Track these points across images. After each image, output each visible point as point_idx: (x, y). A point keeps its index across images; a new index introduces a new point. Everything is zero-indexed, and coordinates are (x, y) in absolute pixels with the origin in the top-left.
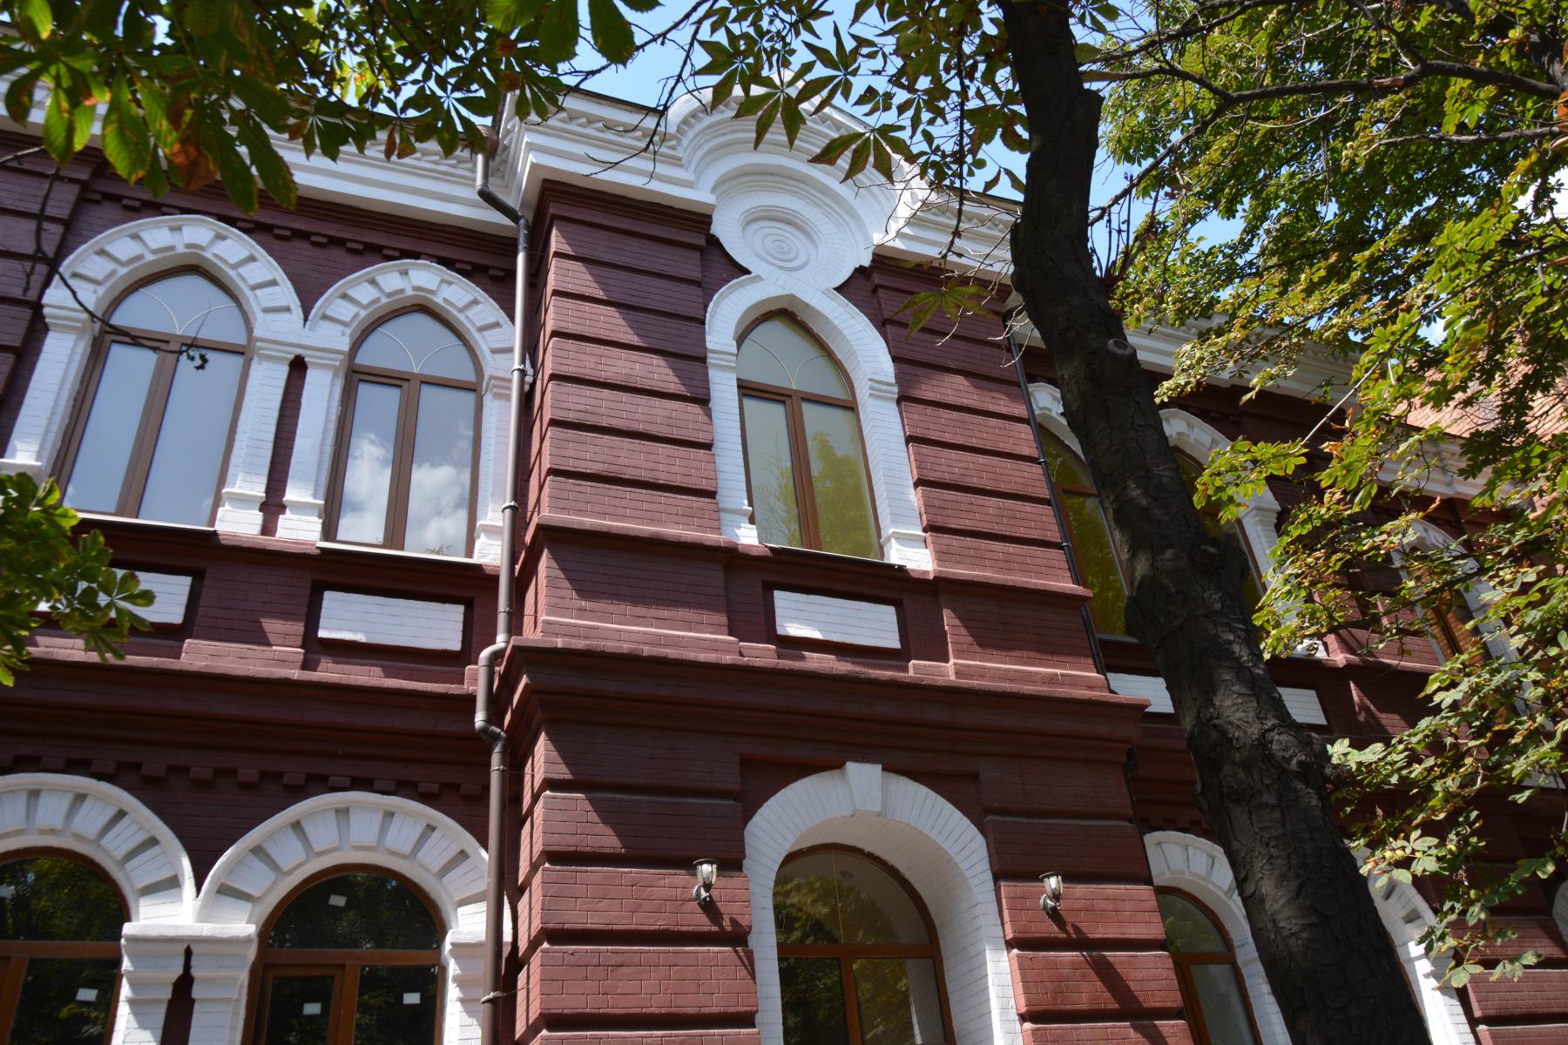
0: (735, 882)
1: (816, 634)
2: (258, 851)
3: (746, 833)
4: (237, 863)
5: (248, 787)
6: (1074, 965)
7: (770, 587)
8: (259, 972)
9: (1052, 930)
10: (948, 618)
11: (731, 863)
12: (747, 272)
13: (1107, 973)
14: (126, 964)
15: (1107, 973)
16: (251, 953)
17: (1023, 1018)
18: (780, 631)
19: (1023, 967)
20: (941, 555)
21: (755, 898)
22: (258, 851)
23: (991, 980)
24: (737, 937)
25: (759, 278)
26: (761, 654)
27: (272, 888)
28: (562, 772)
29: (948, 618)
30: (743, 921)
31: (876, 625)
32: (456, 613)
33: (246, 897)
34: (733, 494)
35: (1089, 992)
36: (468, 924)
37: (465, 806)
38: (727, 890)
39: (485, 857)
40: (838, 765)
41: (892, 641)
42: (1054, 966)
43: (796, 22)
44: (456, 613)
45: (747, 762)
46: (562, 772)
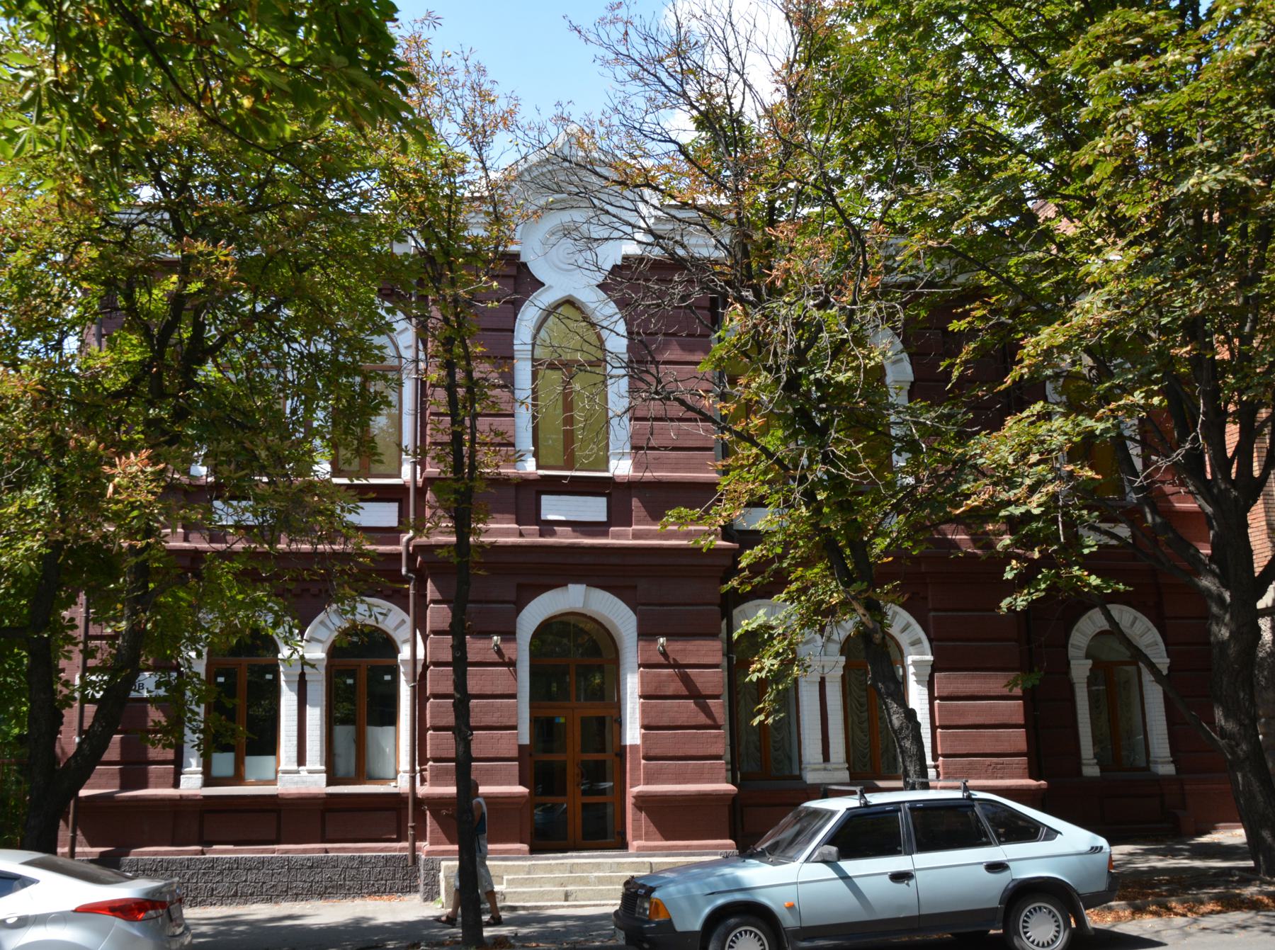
0: (512, 645)
1: (563, 518)
2: (322, 623)
3: (519, 619)
4: (315, 628)
5: (314, 596)
6: (669, 675)
7: (539, 493)
8: (329, 668)
9: (662, 660)
10: (635, 502)
11: (509, 634)
12: (543, 285)
13: (686, 680)
14: (281, 669)
15: (686, 680)
16: (325, 663)
17: (641, 697)
18: (543, 518)
19: (642, 676)
20: (637, 465)
21: (521, 650)
22: (322, 623)
23: (629, 685)
24: (512, 664)
25: (550, 287)
26: (532, 538)
27: (328, 636)
28: (438, 596)
29: (635, 502)
30: (513, 657)
31: (594, 508)
32: (394, 507)
33: (320, 641)
34: (525, 441)
35: (677, 687)
36: (405, 653)
37: (399, 598)
38: (508, 651)
39: (409, 620)
40: (566, 585)
41: (603, 517)
42: (659, 675)
43: (128, 235)
44: (394, 507)
45: (520, 587)
46: (438, 596)
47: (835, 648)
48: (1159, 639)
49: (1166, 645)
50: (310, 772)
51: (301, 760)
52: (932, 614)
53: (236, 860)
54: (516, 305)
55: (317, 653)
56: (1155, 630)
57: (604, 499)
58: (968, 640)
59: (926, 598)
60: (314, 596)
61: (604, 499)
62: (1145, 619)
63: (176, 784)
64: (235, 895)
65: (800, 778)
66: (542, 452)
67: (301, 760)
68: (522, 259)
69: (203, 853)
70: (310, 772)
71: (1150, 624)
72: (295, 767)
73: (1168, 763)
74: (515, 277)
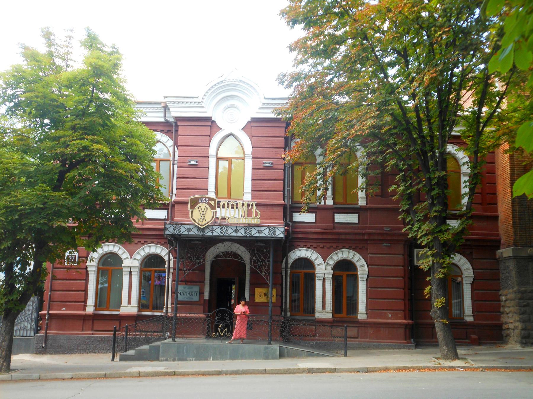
5: (136, 243)
47: (329, 268)
48: (470, 267)
49: (473, 269)
50: (132, 307)
51: (129, 302)
52: (370, 255)
53: (104, 337)
54: (210, 136)
55: (136, 264)
56: (469, 263)
57: (357, 215)
58: (384, 265)
59: (367, 249)
60: (136, 243)
61: (357, 215)
62: (465, 259)
63: (84, 309)
64: (103, 349)
65: (463, 319)
66: (336, 197)
67: (129, 302)
68: (213, 119)
69: (93, 334)
70: (132, 307)
71: (467, 261)
72: (127, 305)
73: (471, 316)
74: (211, 126)
